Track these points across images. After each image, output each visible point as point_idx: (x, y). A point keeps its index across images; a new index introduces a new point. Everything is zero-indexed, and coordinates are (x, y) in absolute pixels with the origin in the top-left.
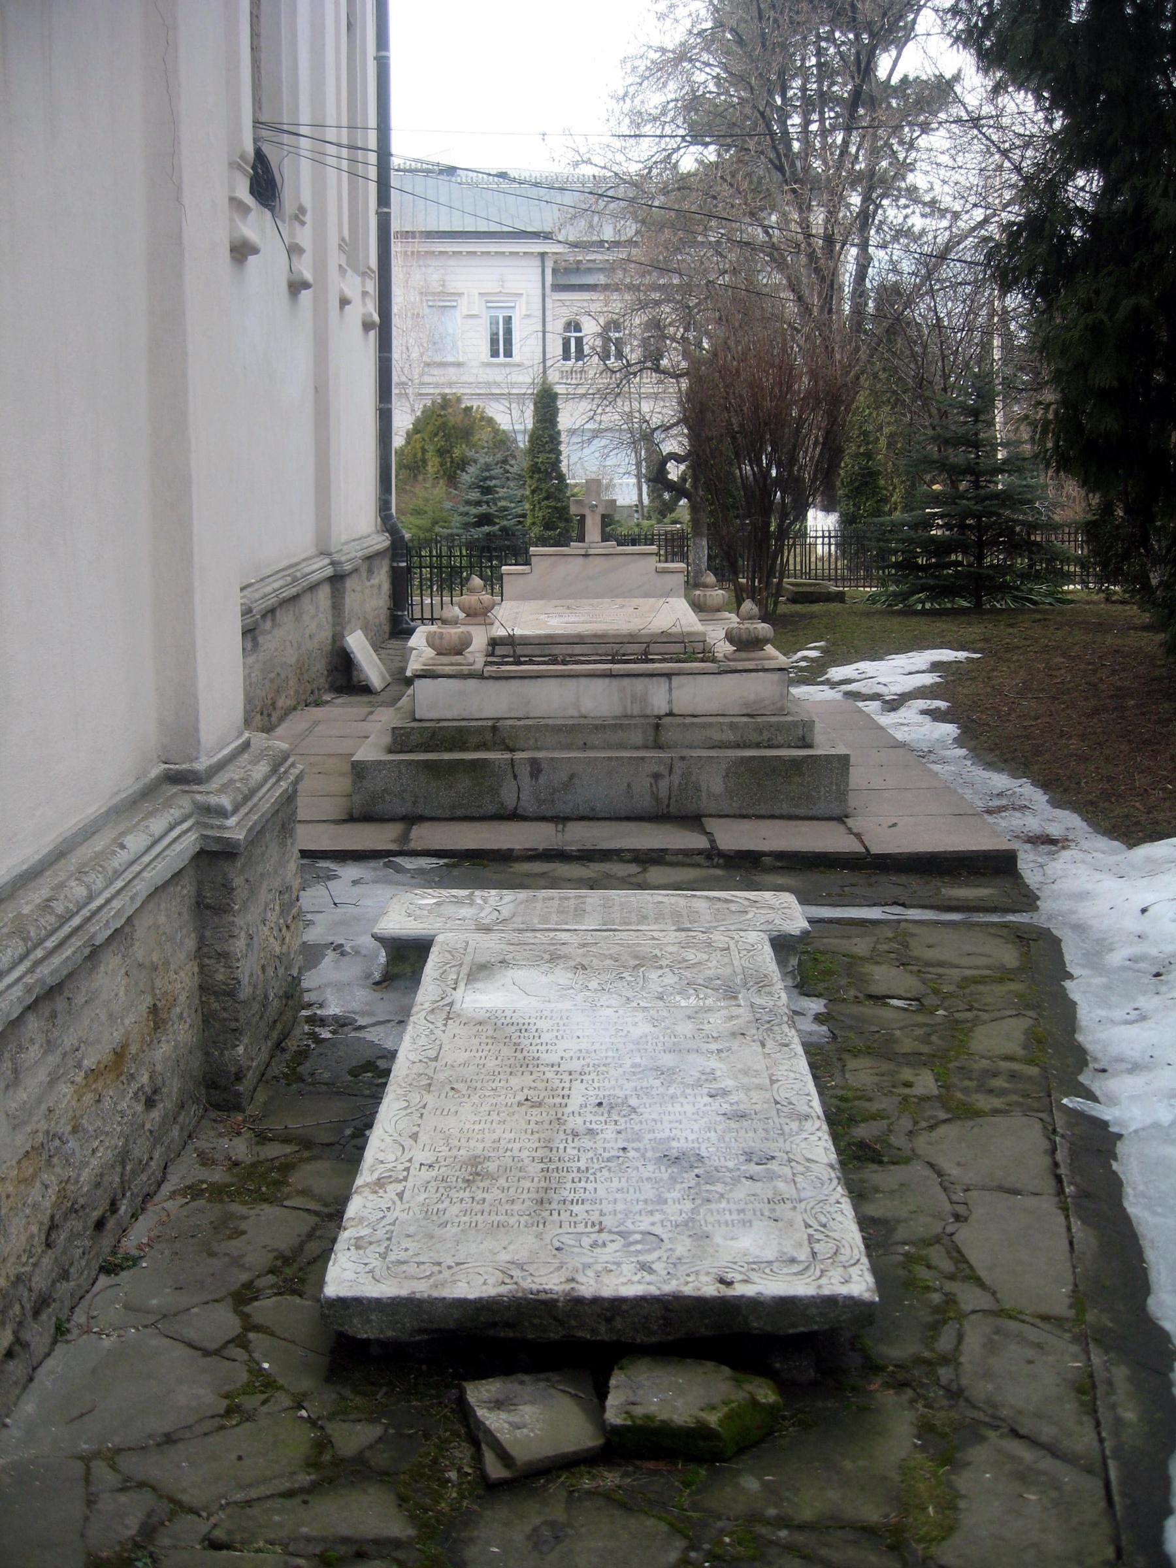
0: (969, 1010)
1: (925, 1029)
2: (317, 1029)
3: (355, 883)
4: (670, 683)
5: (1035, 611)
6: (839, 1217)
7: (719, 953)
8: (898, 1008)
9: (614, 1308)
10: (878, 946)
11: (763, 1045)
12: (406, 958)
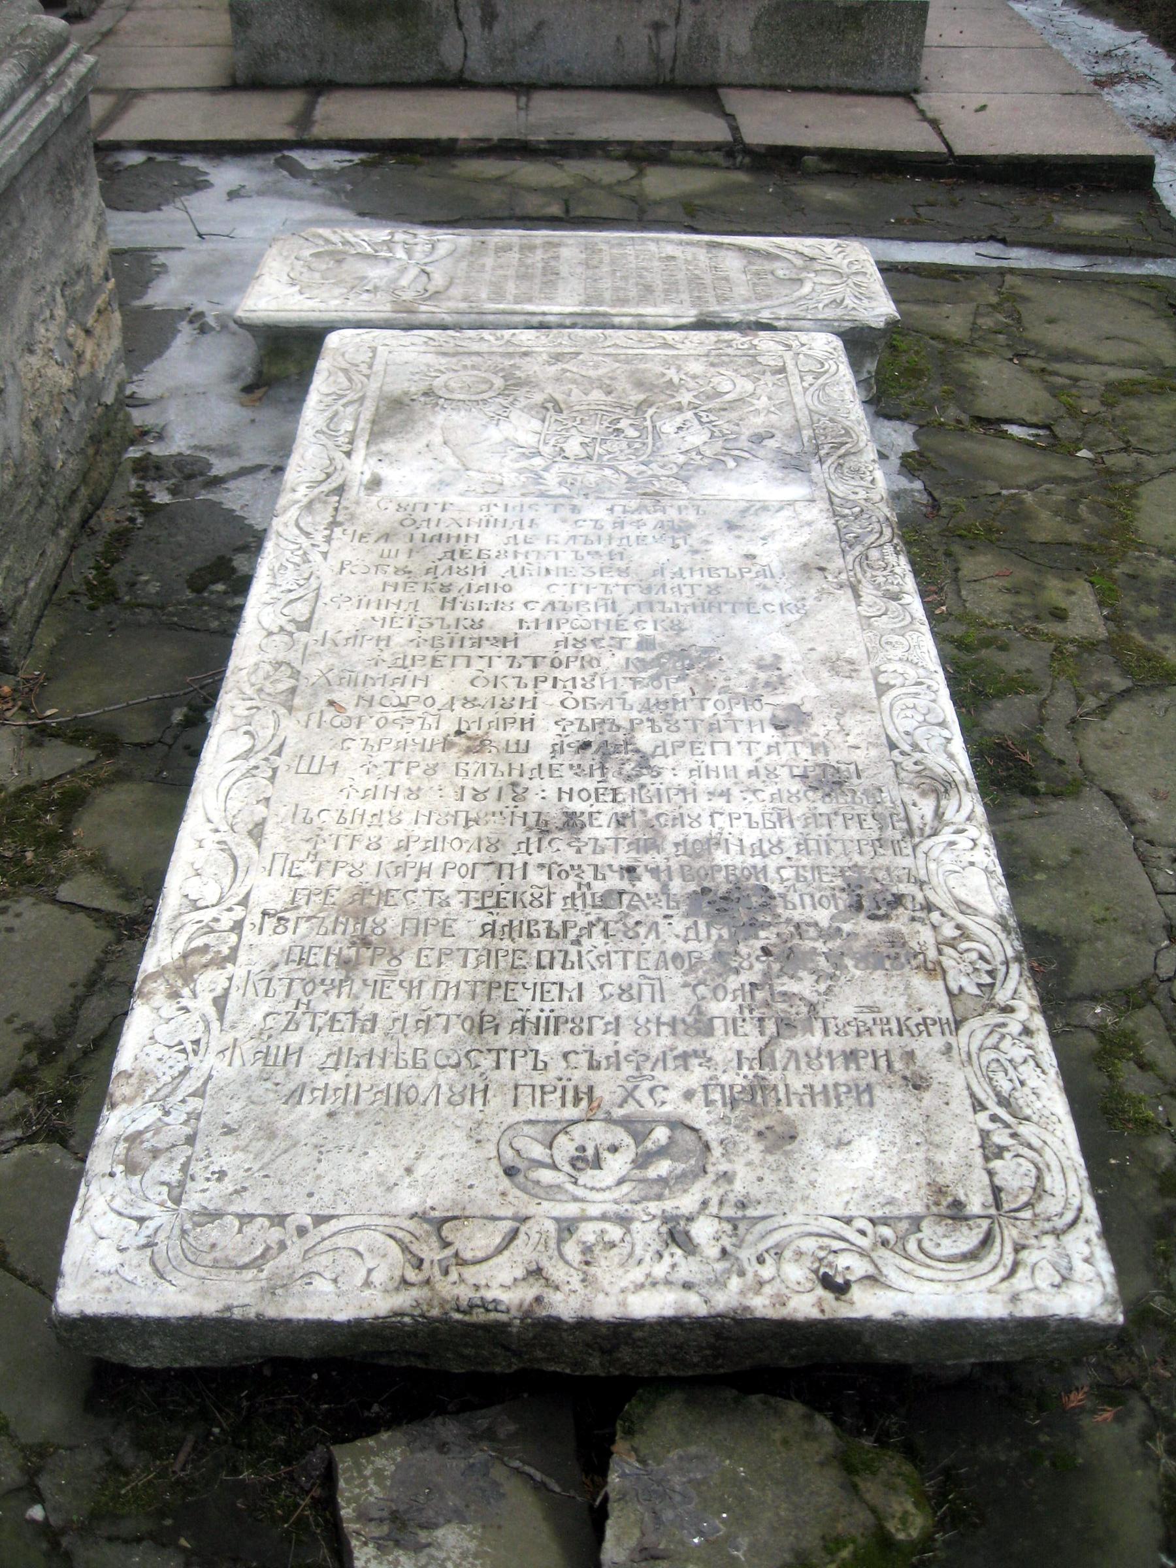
0: (1125, 450)
1: (1067, 488)
2: (148, 487)
3: (233, 195)
6: (1028, 1072)
7: (769, 378)
8: (1020, 441)
9: (624, 1333)
10: (980, 321)
11: (857, 596)
12: (283, 358)
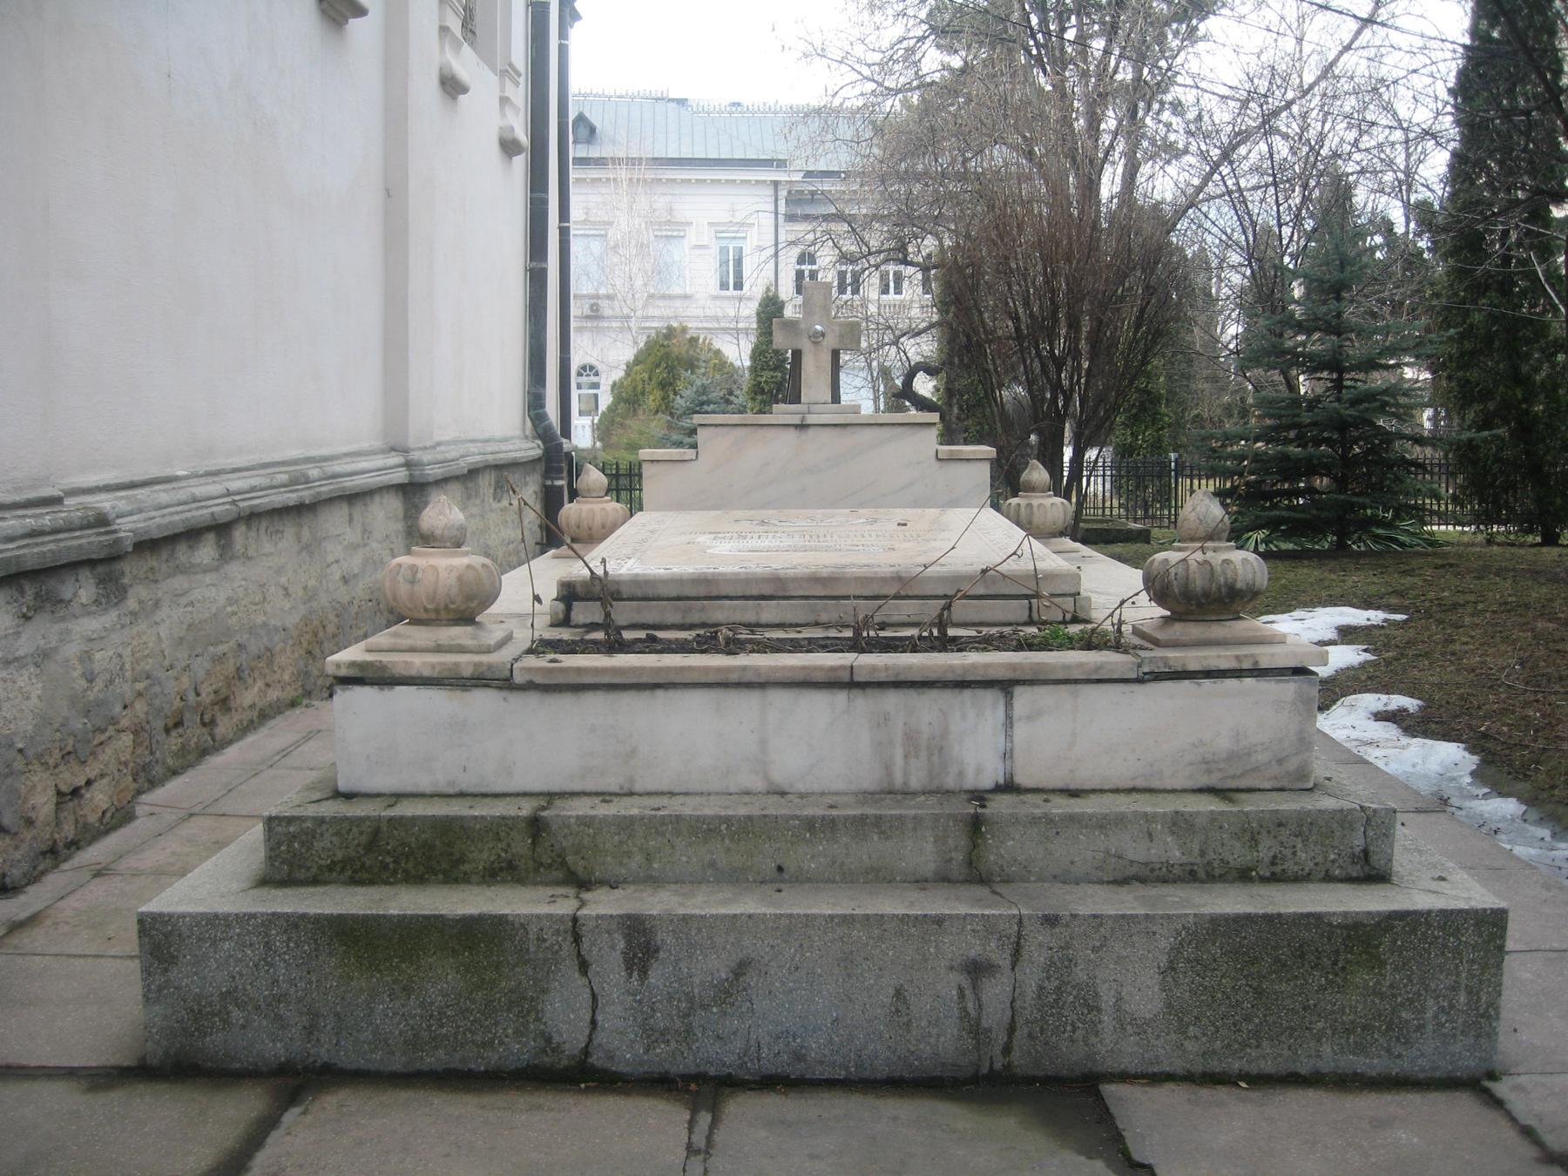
4: (1009, 705)
5: (1435, 554)
